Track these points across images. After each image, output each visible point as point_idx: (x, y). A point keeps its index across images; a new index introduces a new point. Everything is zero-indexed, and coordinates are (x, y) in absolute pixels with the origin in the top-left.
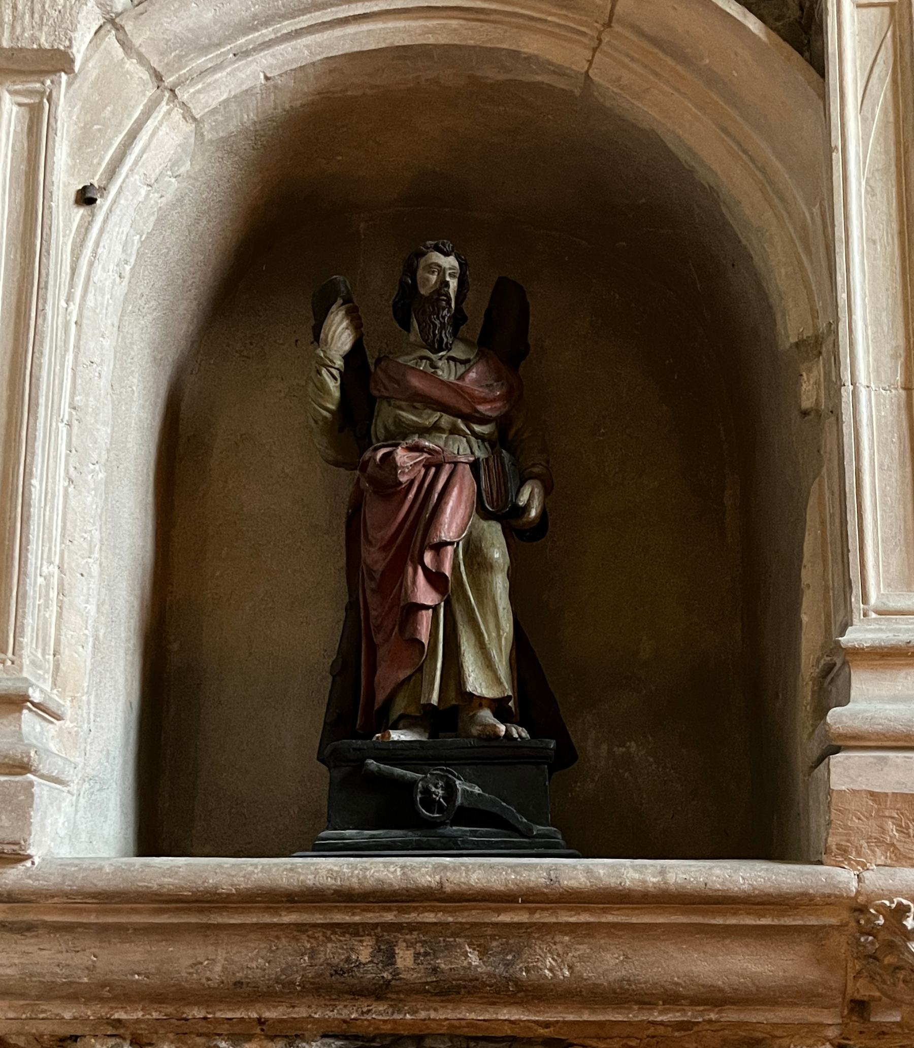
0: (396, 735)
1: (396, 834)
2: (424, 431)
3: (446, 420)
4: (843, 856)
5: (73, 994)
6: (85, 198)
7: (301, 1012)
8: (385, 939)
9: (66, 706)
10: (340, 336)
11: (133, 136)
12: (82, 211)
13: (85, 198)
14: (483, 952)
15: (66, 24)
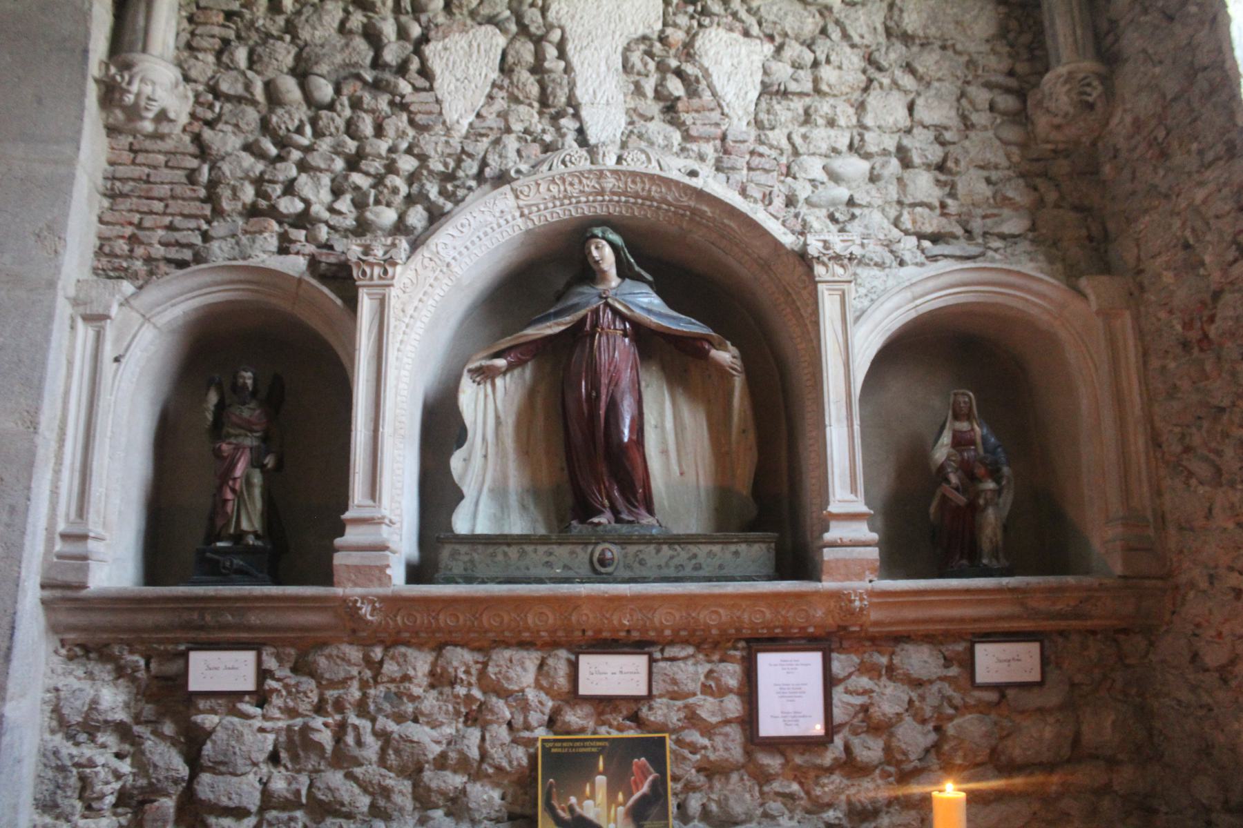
0: (220, 544)
1: (215, 578)
2: (236, 436)
3: (242, 431)
4: (339, 584)
5: (104, 629)
6: (117, 360)
7: (178, 635)
8: (202, 611)
9: (107, 535)
10: (213, 398)
11: (134, 336)
12: (115, 365)
13: (117, 360)
14: (233, 616)
15: (108, 307)
